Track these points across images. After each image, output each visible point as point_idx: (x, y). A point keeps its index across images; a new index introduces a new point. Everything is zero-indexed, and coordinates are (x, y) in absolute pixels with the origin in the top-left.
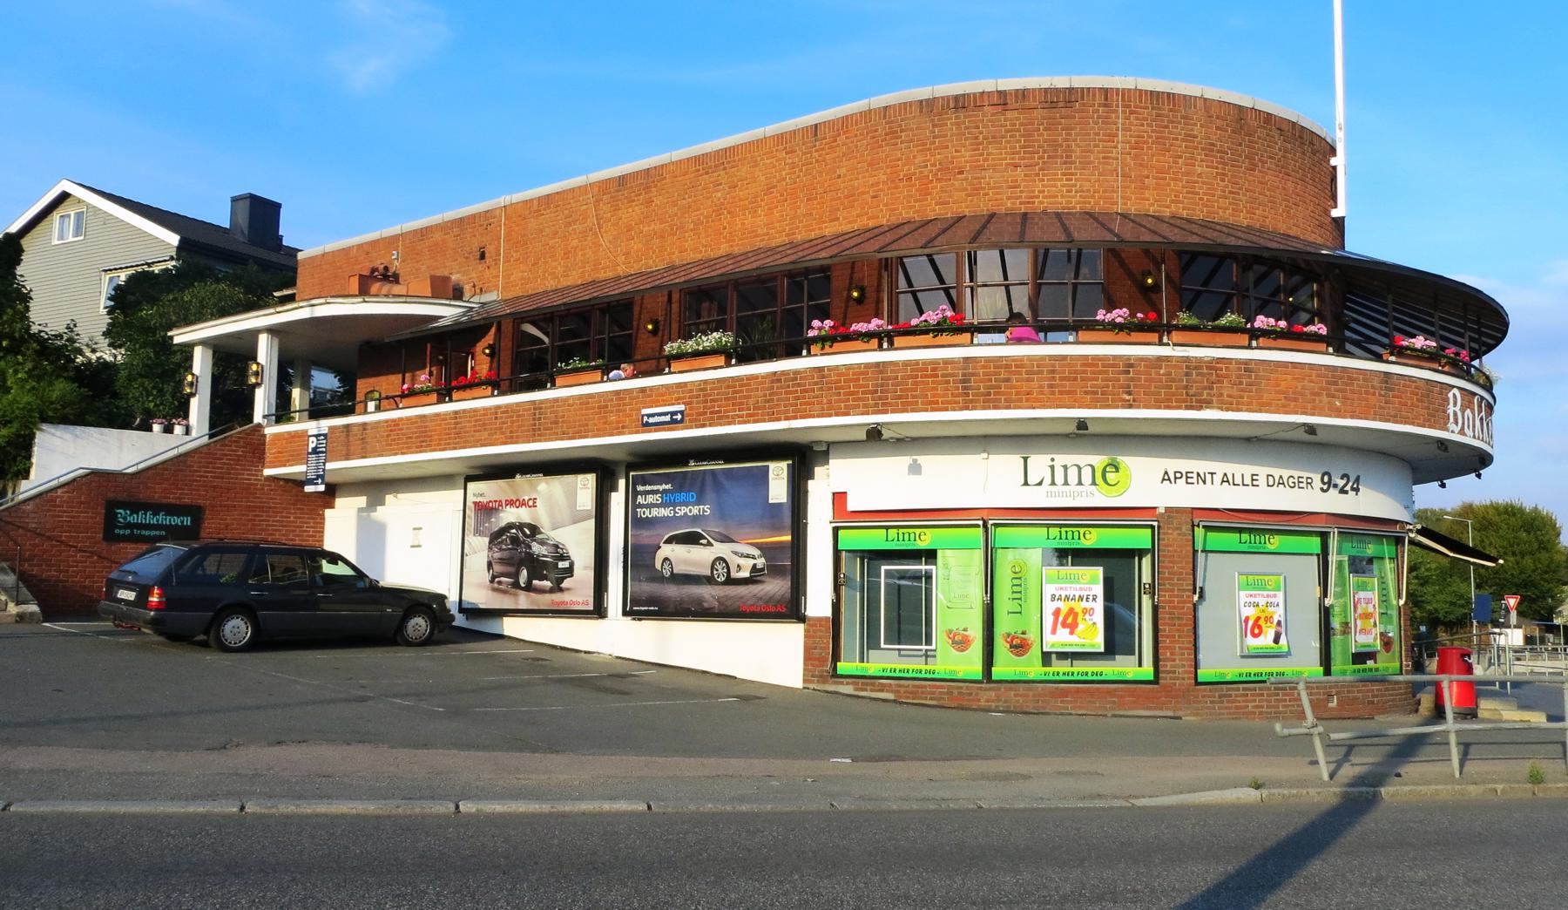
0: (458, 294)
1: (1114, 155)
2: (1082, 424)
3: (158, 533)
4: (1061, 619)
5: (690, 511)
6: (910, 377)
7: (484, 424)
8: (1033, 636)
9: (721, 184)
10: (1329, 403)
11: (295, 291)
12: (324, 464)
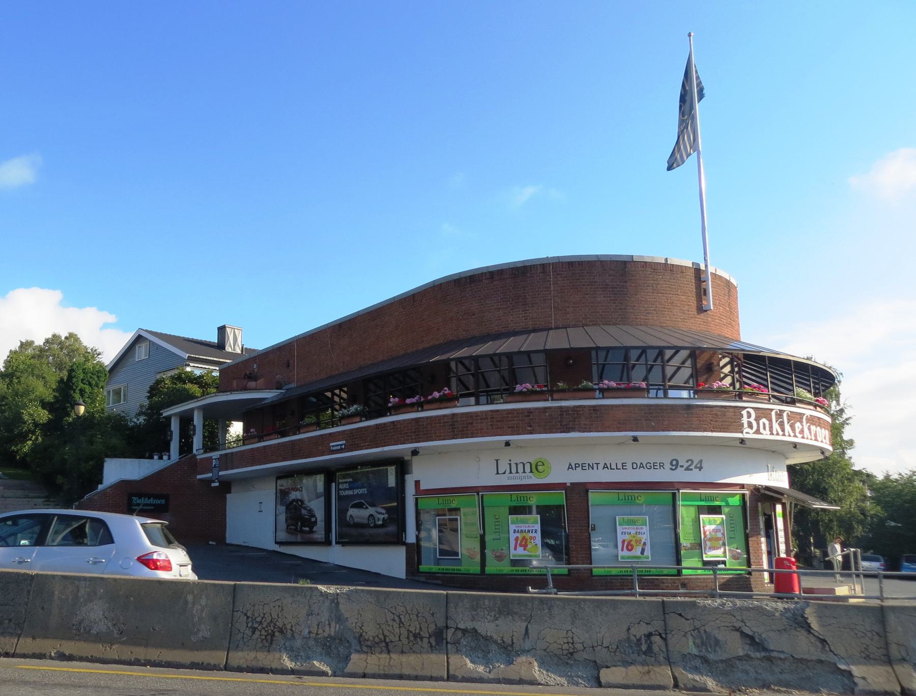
1: (549, 298)
3: (150, 507)
4: (519, 542)
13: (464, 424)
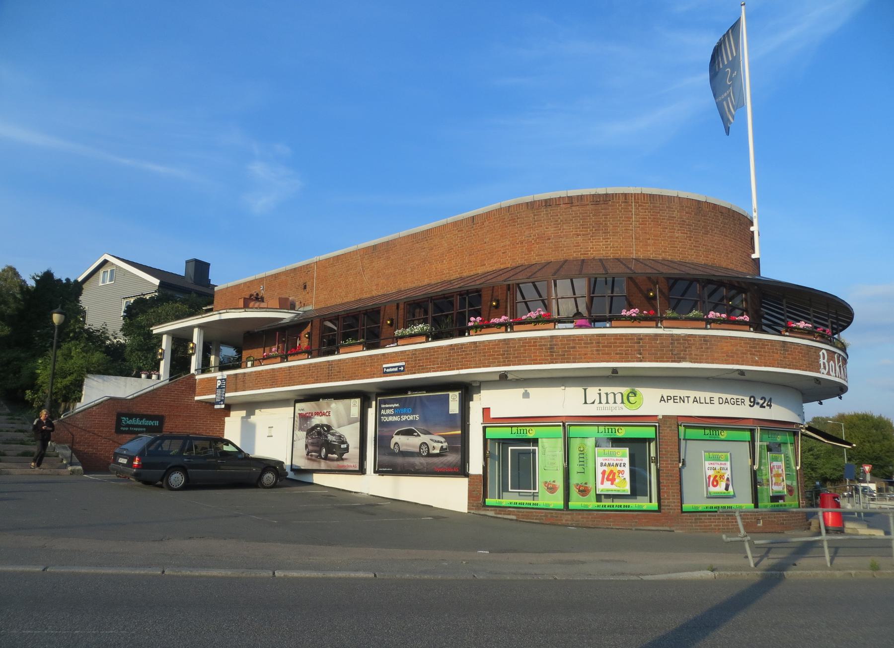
0: (292, 307)
2: (615, 370)
4: (606, 476)
5: (409, 418)
6: (522, 346)
7: (303, 373)
8: (591, 485)
9: (425, 248)
10: (752, 358)
11: (213, 307)
12: (224, 394)
13: (565, 348)
